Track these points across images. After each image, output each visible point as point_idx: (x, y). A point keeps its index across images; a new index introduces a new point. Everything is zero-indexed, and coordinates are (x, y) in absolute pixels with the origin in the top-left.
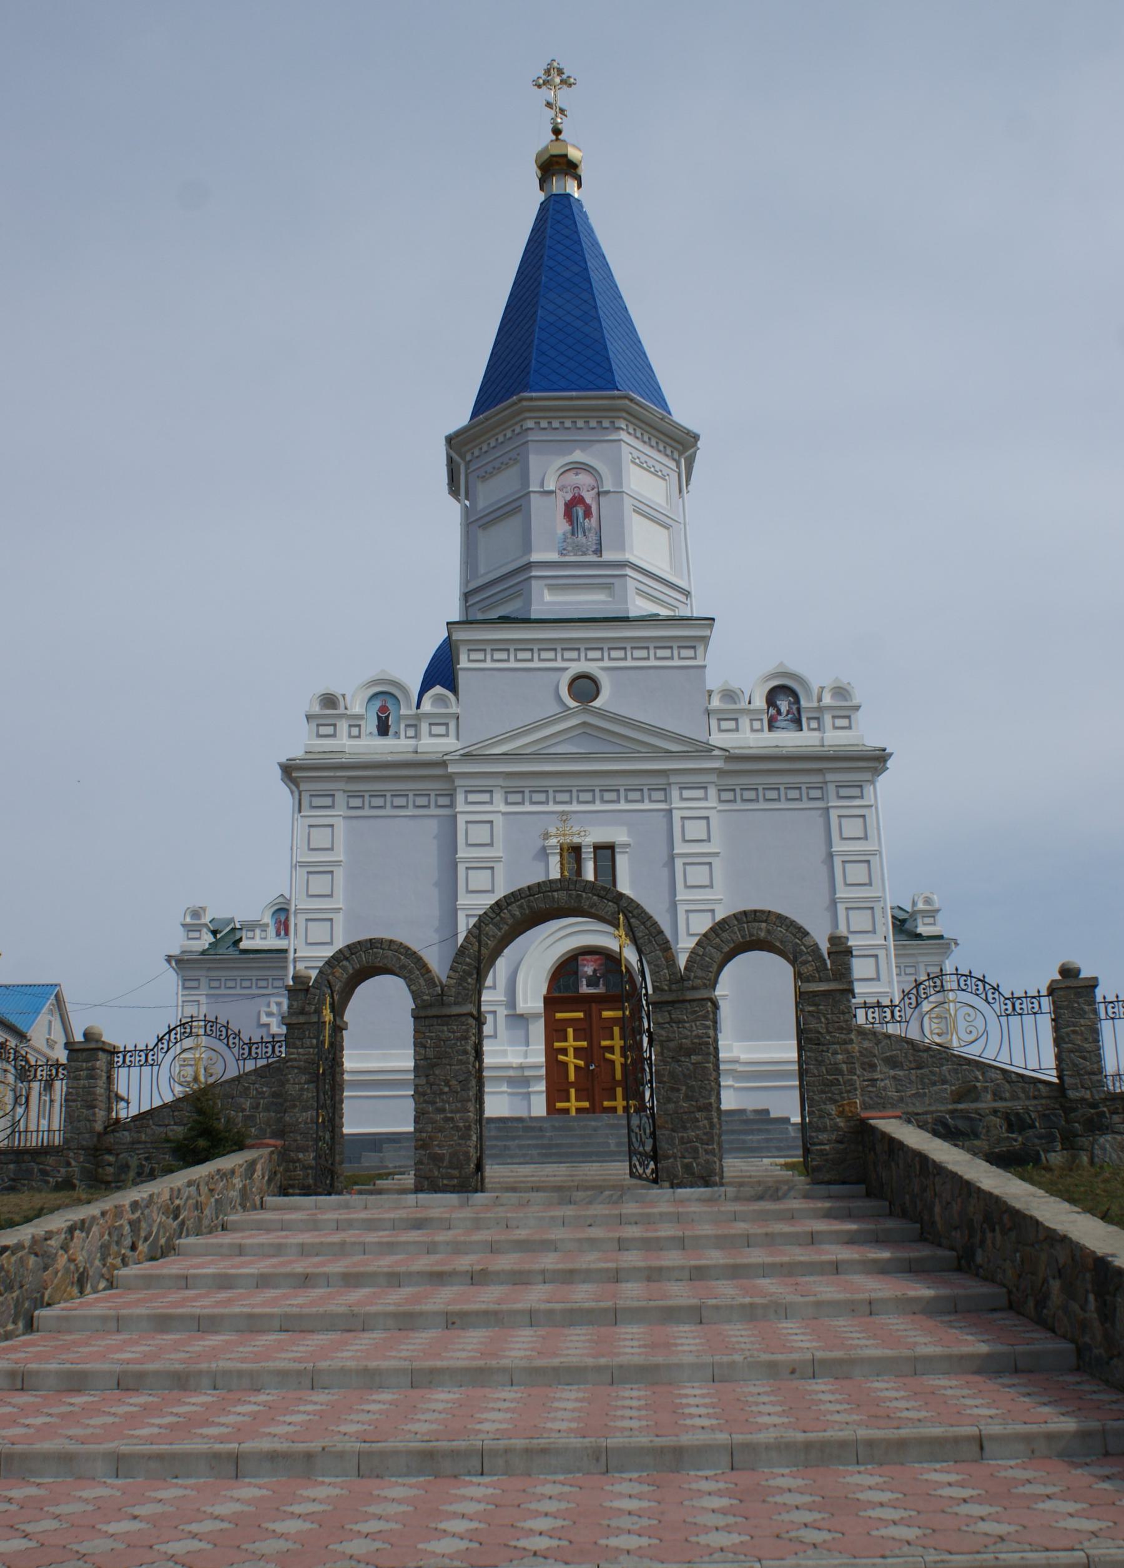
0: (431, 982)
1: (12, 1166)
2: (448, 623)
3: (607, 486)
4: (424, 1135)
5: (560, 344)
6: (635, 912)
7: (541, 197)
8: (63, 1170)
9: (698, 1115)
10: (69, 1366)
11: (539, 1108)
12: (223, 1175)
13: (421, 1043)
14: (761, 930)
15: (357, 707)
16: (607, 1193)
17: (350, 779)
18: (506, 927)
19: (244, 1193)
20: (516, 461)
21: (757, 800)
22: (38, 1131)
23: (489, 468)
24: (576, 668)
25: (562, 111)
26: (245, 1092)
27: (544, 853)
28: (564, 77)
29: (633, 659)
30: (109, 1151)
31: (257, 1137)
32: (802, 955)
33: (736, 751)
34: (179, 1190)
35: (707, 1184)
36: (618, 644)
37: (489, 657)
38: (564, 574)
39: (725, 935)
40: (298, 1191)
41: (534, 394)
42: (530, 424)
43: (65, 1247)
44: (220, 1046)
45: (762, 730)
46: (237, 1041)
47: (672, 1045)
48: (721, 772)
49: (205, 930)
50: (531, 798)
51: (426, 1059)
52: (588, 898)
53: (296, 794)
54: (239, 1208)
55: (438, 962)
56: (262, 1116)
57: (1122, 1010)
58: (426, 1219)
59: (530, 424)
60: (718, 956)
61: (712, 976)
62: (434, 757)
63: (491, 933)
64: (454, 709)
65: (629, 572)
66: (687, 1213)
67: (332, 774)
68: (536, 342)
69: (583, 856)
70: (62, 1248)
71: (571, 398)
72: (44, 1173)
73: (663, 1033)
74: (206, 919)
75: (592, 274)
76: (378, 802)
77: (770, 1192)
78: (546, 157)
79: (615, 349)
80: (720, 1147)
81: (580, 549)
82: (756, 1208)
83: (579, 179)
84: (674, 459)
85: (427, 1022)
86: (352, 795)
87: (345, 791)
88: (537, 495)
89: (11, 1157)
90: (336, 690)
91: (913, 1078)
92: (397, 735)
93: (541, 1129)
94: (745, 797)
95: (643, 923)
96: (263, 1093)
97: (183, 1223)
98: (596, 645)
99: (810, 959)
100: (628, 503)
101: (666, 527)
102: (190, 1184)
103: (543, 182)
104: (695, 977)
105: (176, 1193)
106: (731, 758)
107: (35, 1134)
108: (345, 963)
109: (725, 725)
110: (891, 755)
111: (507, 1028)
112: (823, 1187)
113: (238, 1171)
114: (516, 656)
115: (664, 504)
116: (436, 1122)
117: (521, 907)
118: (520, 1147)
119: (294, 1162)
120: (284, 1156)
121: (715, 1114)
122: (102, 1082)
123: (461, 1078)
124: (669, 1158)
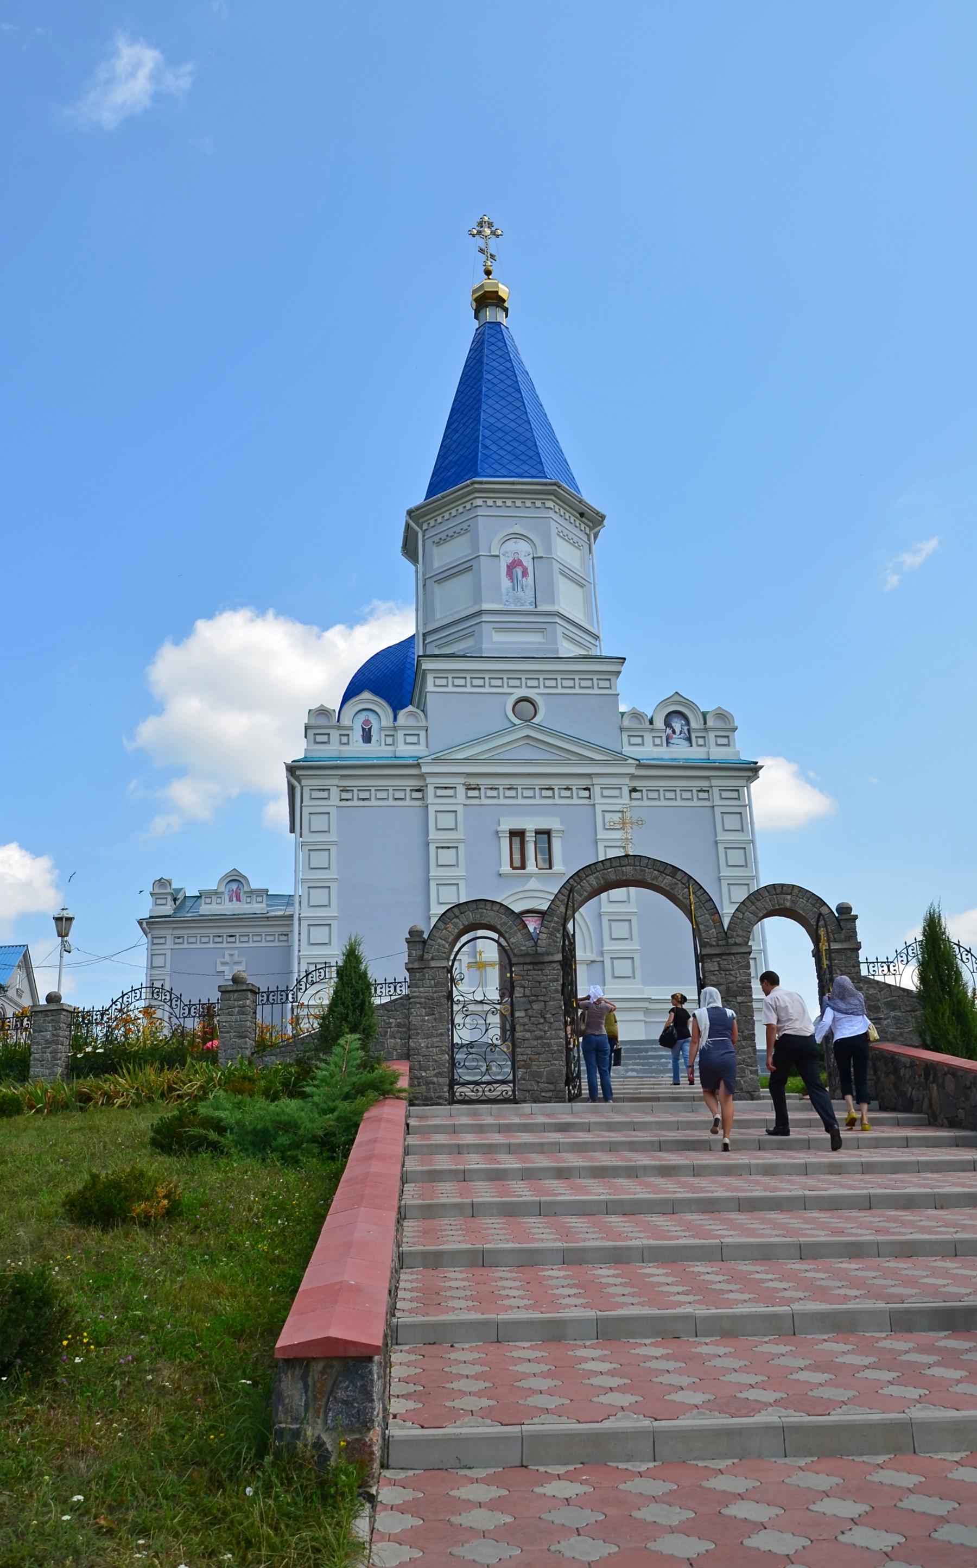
5: (489, 438)
7: (476, 324)
10: (422, 1248)
20: (467, 531)
25: (492, 256)
28: (493, 229)
38: (513, 619)
39: (758, 904)
42: (479, 502)
45: (662, 745)
57: (975, 966)
83: (506, 310)
91: (910, 1018)
100: (556, 566)
108: (455, 920)
110: (761, 767)
115: (578, 567)
117: (596, 878)
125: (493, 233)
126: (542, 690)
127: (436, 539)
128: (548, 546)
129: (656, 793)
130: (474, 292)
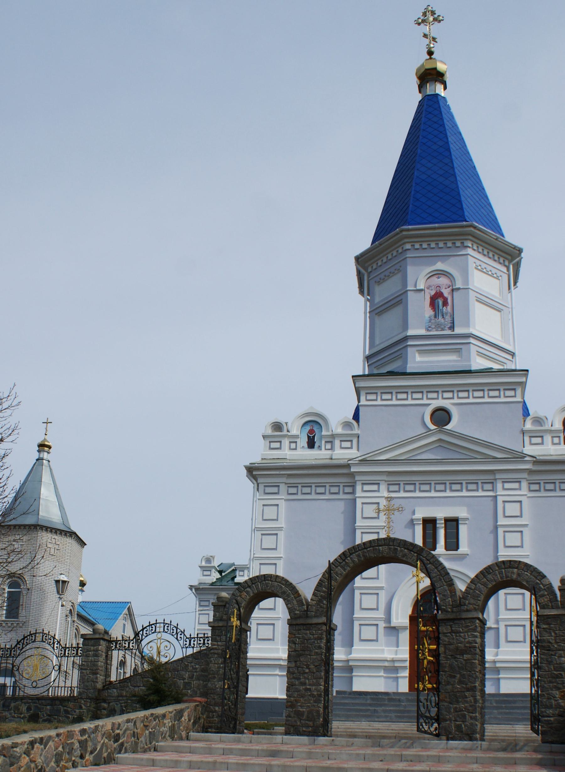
0: (300, 603)
1: (48, 707)
2: (353, 377)
3: (459, 285)
4: (292, 699)
6: (431, 560)
7: (419, 97)
8: (77, 711)
9: (467, 694)
11: (404, 687)
12: (156, 717)
13: (293, 641)
14: (514, 574)
15: (295, 431)
16: (403, 741)
17: (290, 476)
18: (348, 569)
19: (172, 730)
21: (554, 490)
22: (58, 687)
23: (382, 276)
24: (435, 404)
25: (434, 39)
26: (186, 668)
27: (412, 523)
28: (436, 16)
29: (474, 397)
30: (104, 701)
31: (191, 696)
32: (540, 591)
33: (541, 458)
34: (119, 724)
35: (471, 739)
36: (465, 388)
37: (379, 398)
38: (429, 344)
39: (490, 577)
40: (214, 730)
41: (410, 227)
42: (408, 246)
43: (27, 753)
44: (172, 639)
45: (559, 444)
46: (182, 636)
47: (452, 647)
48: (530, 472)
49: (213, 570)
50: (435, 487)
51: (295, 651)
52: (401, 551)
53: (256, 485)
54: (168, 738)
55: (307, 590)
56: (195, 683)
58: (278, 751)
59: (408, 246)
60: (485, 590)
61: (480, 603)
62: (342, 462)
63: (339, 572)
64: (356, 431)
65: (472, 340)
66: (445, 756)
67: (278, 473)
68: (413, 193)
69: (438, 526)
70: (25, 753)
71: (435, 228)
72: (67, 712)
73: (446, 639)
74: (216, 563)
75: (451, 146)
76: (307, 490)
77: (511, 746)
78: (423, 70)
79: (466, 195)
80: (483, 715)
81: (439, 327)
82: (490, 755)
84: (505, 266)
85: (297, 627)
86: (290, 486)
87: (286, 484)
88: (412, 292)
89: (49, 702)
90: (282, 419)
92: (320, 447)
93: (399, 700)
94: (547, 488)
95: (436, 568)
96: (196, 669)
97: (122, 744)
98: (449, 388)
99: (546, 593)
100: (472, 295)
101: (499, 311)
102: (128, 721)
103: (421, 87)
104: (469, 604)
105: (117, 726)
106: (537, 462)
107: (63, 689)
108: (248, 589)
109: (534, 440)
111: (385, 636)
112: (548, 745)
113: (168, 716)
114: (396, 397)
116: (299, 691)
117: (358, 556)
118: (385, 711)
119: (213, 712)
120: (206, 708)
121: (478, 693)
122: (102, 659)
123: (316, 664)
124: (446, 721)
125: (435, 20)
126: (456, 401)
127: (377, 279)
128: (466, 279)
129: (552, 485)
130: (418, 70)
